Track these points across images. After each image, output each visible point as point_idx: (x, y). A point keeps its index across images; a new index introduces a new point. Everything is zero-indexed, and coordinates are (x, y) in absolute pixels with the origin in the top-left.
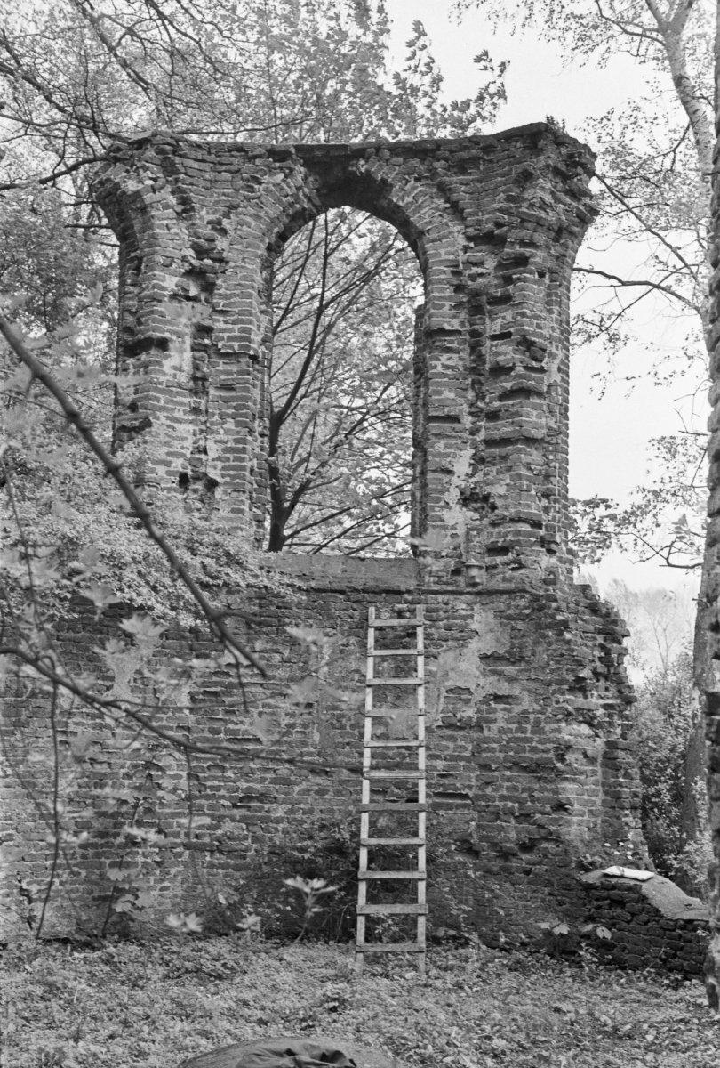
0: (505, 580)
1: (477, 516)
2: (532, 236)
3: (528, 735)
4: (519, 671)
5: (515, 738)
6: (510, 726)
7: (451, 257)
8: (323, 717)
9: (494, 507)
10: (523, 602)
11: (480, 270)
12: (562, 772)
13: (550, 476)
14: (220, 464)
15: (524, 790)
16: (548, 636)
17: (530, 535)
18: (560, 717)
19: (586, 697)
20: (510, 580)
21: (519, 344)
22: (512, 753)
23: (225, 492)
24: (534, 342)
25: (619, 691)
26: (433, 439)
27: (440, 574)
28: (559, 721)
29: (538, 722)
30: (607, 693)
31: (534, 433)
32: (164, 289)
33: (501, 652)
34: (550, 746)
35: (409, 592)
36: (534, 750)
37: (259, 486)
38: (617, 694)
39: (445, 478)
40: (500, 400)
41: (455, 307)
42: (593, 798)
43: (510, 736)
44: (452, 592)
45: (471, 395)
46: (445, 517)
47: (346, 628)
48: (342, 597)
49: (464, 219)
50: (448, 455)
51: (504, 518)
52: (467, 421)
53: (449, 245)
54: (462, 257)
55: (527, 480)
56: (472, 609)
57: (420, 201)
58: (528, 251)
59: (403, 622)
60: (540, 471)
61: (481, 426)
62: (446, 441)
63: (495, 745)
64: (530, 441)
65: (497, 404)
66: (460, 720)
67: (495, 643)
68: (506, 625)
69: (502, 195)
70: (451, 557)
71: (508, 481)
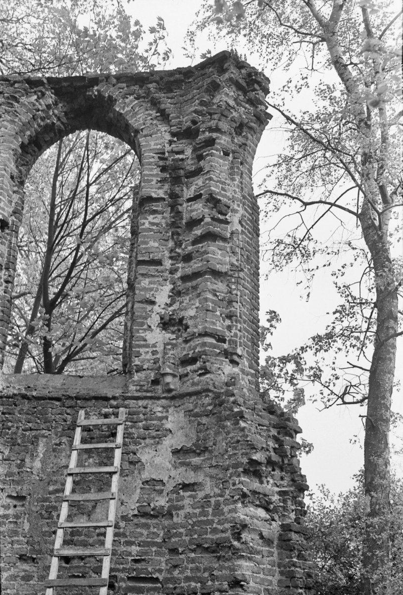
0: (193, 384)
1: (174, 336)
2: (217, 123)
3: (210, 518)
4: (203, 460)
5: (198, 521)
6: (195, 511)
7: (159, 147)
8: (34, 509)
9: (187, 327)
10: (207, 400)
11: (181, 156)
12: (238, 549)
13: (232, 301)
15: (205, 570)
16: (227, 426)
18: (236, 497)
19: (261, 482)
20: (197, 384)
21: (208, 201)
22: (196, 536)
24: (220, 200)
25: (293, 480)
26: (140, 278)
27: (142, 383)
28: (235, 502)
29: (218, 504)
30: (282, 482)
31: (218, 267)
33: (189, 445)
34: (228, 526)
35: (114, 398)
36: (215, 531)
38: (291, 483)
39: (149, 308)
41: (160, 181)
42: (270, 578)
43: (194, 520)
44: (151, 398)
45: (171, 244)
46: (147, 338)
47: (60, 430)
48: (58, 403)
49: (169, 121)
50: (151, 289)
52: (168, 264)
53: (157, 139)
54: (168, 148)
56: (167, 411)
57: (137, 109)
58: (214, 135)
59: (107, 421)
61: (178, 267)
62: (150, 279)
63: (182, 530)
64: (216, 274)
65: (190, 248)
66: (153, 510)
67: (184, 439)
68: (193, 422)
69: (197, 101)
70: (151, 370)
71: (197, 305)
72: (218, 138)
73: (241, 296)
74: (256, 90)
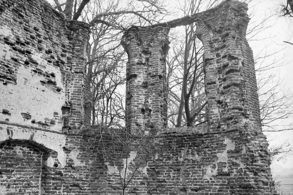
3: (243, 176)
7: (209, 39)
10: (237, 134)
13: (243, 94)
14: (152, 105)
17: (238, 113)
22: (239, 183)
23: (153, 112)
32: (135, 62)
36: (245, 181)
37: (164, 110)
40: (226, 75)
51: (230, 109)
55: (236, 96)
56: (224, 138)
58: (228, 32)
60: (240, 93)
63: (234, 180)
64: (236, 85)
70: (217, 123)
71: (230, 97)
72: (230, 33)
73: (246, 92)
74: (243, 10)
